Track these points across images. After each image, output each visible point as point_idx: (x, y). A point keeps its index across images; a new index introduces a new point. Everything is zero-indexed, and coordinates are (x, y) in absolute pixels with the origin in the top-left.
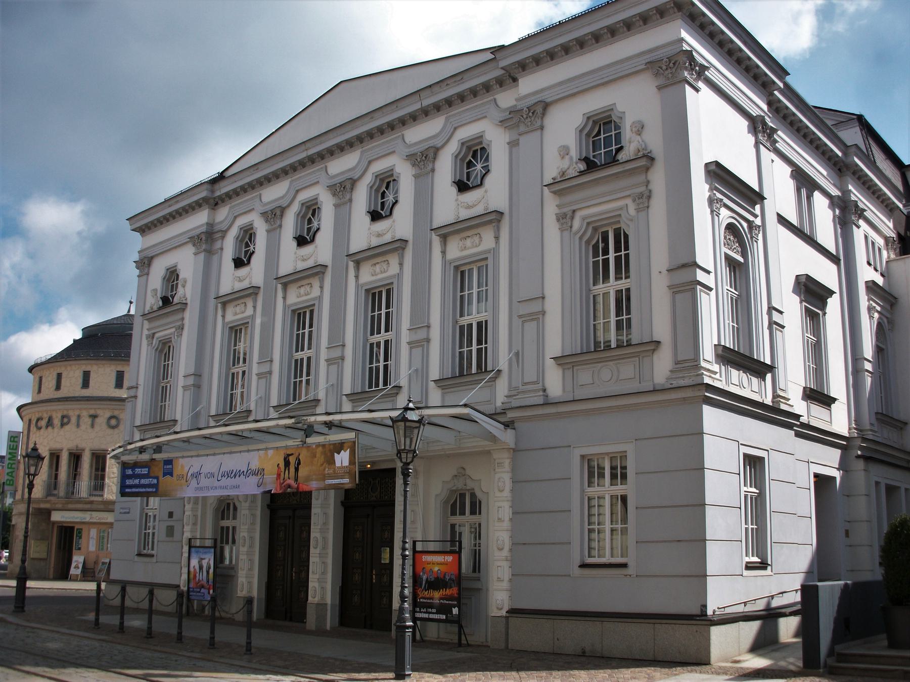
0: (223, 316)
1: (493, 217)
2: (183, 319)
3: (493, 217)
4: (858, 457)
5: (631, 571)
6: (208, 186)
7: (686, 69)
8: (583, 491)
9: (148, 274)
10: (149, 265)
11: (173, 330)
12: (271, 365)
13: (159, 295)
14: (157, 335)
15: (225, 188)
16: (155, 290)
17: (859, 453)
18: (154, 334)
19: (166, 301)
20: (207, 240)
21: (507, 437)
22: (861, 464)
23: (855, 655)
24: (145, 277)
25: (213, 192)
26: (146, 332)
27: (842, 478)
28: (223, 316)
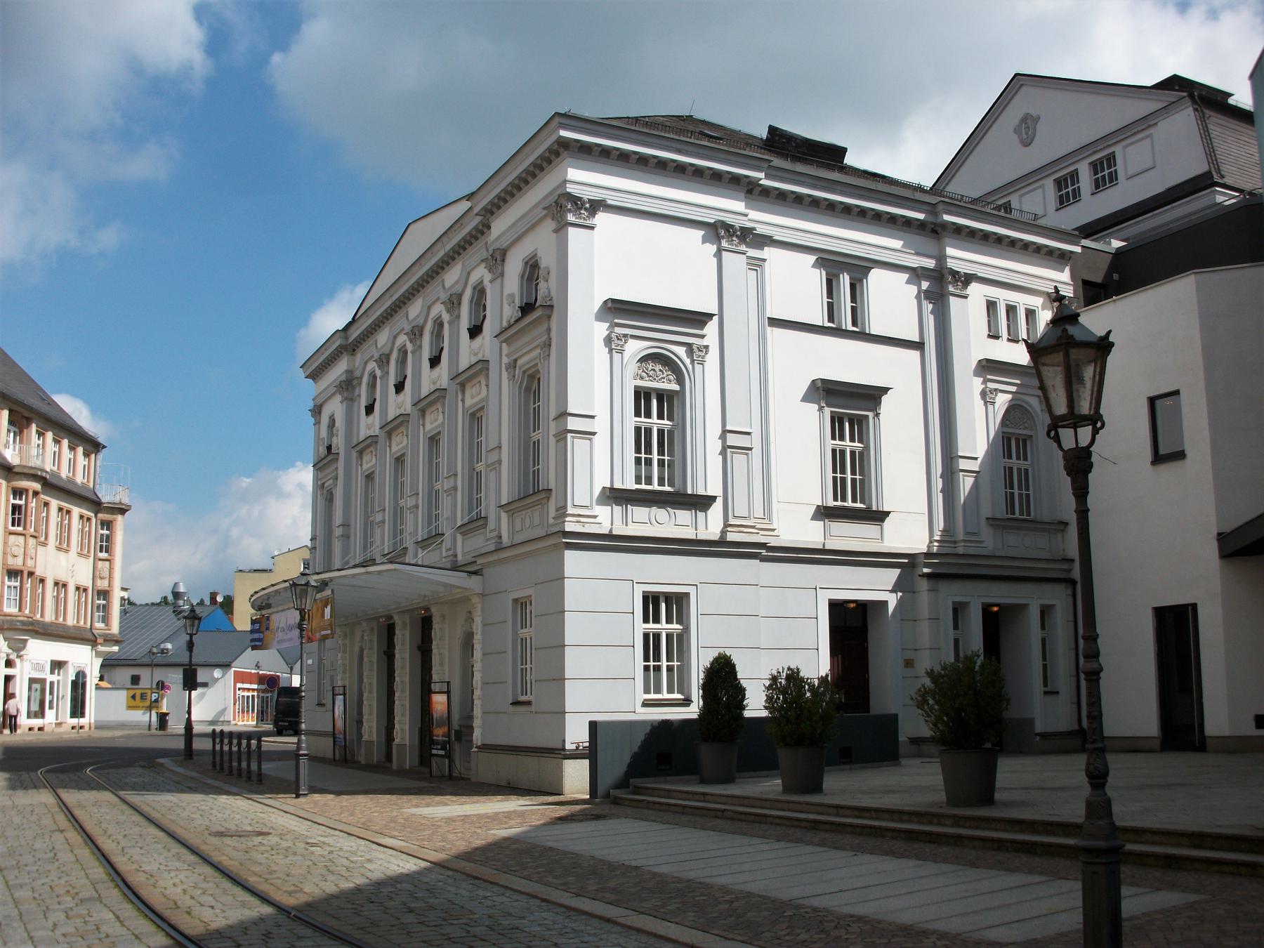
0: (463, 401)
1: (479, 366)
2: (549, 330)
3: (479, 366)
4: (928, 576)
5: (533, 708)
6: (342, 334)
7: (570, 211)
8: (515, 633)
9: (502, 275)
10: (320, 413)
11: (538, 351)
12: (500, 453)
13: (518, 303)
14: (520, 362)
15: (355, 333)
16: (511, 296)
17: (926, 570)
18: (516, 360)
19: (527, 308)
20: (348, 386)
21: (474, 583)
22: (924, 585)
23: (647, 788)
24: (499, 280)
25: (347, 338)
26: (505, 360)
27: (900, 603)
28: (463, 401)
